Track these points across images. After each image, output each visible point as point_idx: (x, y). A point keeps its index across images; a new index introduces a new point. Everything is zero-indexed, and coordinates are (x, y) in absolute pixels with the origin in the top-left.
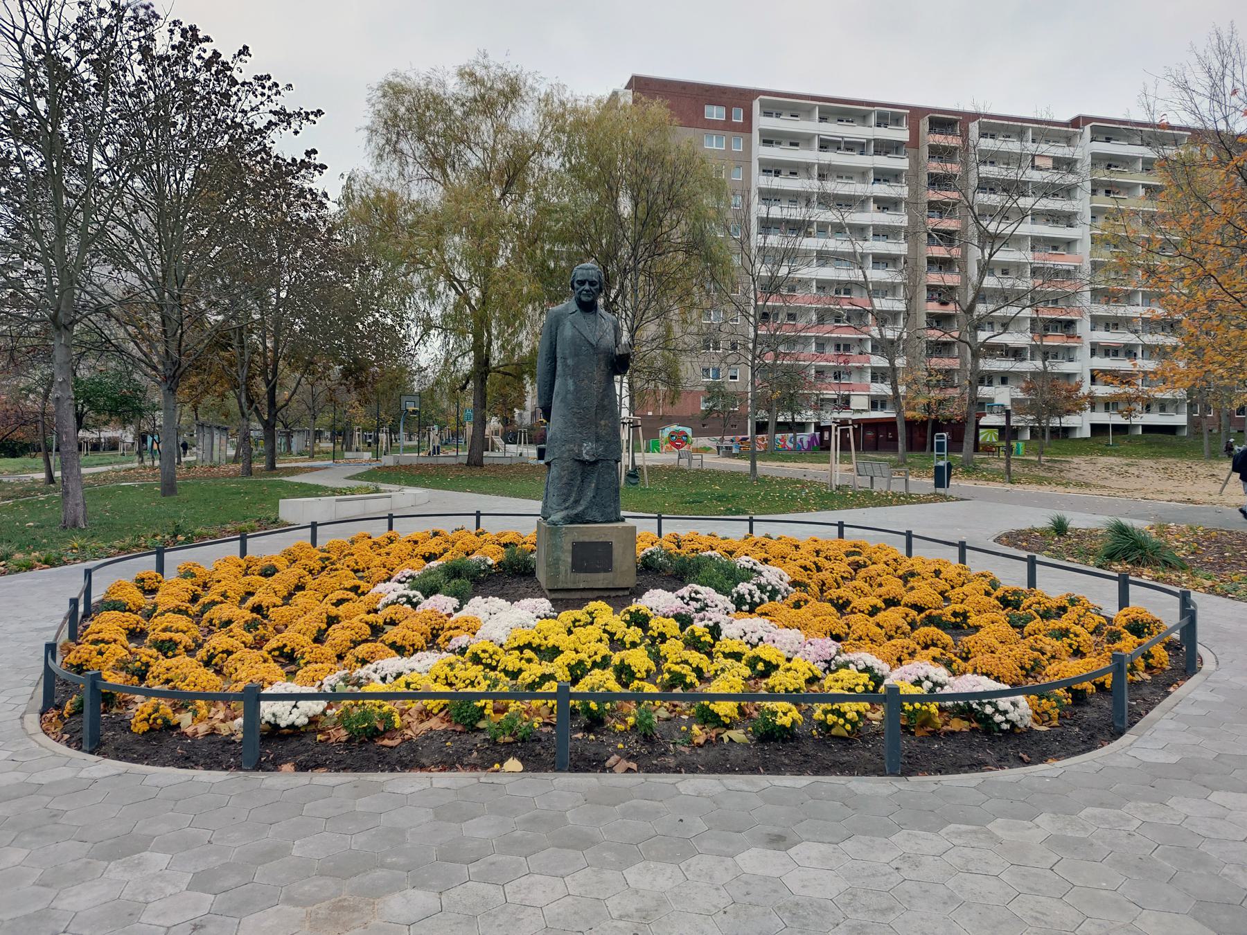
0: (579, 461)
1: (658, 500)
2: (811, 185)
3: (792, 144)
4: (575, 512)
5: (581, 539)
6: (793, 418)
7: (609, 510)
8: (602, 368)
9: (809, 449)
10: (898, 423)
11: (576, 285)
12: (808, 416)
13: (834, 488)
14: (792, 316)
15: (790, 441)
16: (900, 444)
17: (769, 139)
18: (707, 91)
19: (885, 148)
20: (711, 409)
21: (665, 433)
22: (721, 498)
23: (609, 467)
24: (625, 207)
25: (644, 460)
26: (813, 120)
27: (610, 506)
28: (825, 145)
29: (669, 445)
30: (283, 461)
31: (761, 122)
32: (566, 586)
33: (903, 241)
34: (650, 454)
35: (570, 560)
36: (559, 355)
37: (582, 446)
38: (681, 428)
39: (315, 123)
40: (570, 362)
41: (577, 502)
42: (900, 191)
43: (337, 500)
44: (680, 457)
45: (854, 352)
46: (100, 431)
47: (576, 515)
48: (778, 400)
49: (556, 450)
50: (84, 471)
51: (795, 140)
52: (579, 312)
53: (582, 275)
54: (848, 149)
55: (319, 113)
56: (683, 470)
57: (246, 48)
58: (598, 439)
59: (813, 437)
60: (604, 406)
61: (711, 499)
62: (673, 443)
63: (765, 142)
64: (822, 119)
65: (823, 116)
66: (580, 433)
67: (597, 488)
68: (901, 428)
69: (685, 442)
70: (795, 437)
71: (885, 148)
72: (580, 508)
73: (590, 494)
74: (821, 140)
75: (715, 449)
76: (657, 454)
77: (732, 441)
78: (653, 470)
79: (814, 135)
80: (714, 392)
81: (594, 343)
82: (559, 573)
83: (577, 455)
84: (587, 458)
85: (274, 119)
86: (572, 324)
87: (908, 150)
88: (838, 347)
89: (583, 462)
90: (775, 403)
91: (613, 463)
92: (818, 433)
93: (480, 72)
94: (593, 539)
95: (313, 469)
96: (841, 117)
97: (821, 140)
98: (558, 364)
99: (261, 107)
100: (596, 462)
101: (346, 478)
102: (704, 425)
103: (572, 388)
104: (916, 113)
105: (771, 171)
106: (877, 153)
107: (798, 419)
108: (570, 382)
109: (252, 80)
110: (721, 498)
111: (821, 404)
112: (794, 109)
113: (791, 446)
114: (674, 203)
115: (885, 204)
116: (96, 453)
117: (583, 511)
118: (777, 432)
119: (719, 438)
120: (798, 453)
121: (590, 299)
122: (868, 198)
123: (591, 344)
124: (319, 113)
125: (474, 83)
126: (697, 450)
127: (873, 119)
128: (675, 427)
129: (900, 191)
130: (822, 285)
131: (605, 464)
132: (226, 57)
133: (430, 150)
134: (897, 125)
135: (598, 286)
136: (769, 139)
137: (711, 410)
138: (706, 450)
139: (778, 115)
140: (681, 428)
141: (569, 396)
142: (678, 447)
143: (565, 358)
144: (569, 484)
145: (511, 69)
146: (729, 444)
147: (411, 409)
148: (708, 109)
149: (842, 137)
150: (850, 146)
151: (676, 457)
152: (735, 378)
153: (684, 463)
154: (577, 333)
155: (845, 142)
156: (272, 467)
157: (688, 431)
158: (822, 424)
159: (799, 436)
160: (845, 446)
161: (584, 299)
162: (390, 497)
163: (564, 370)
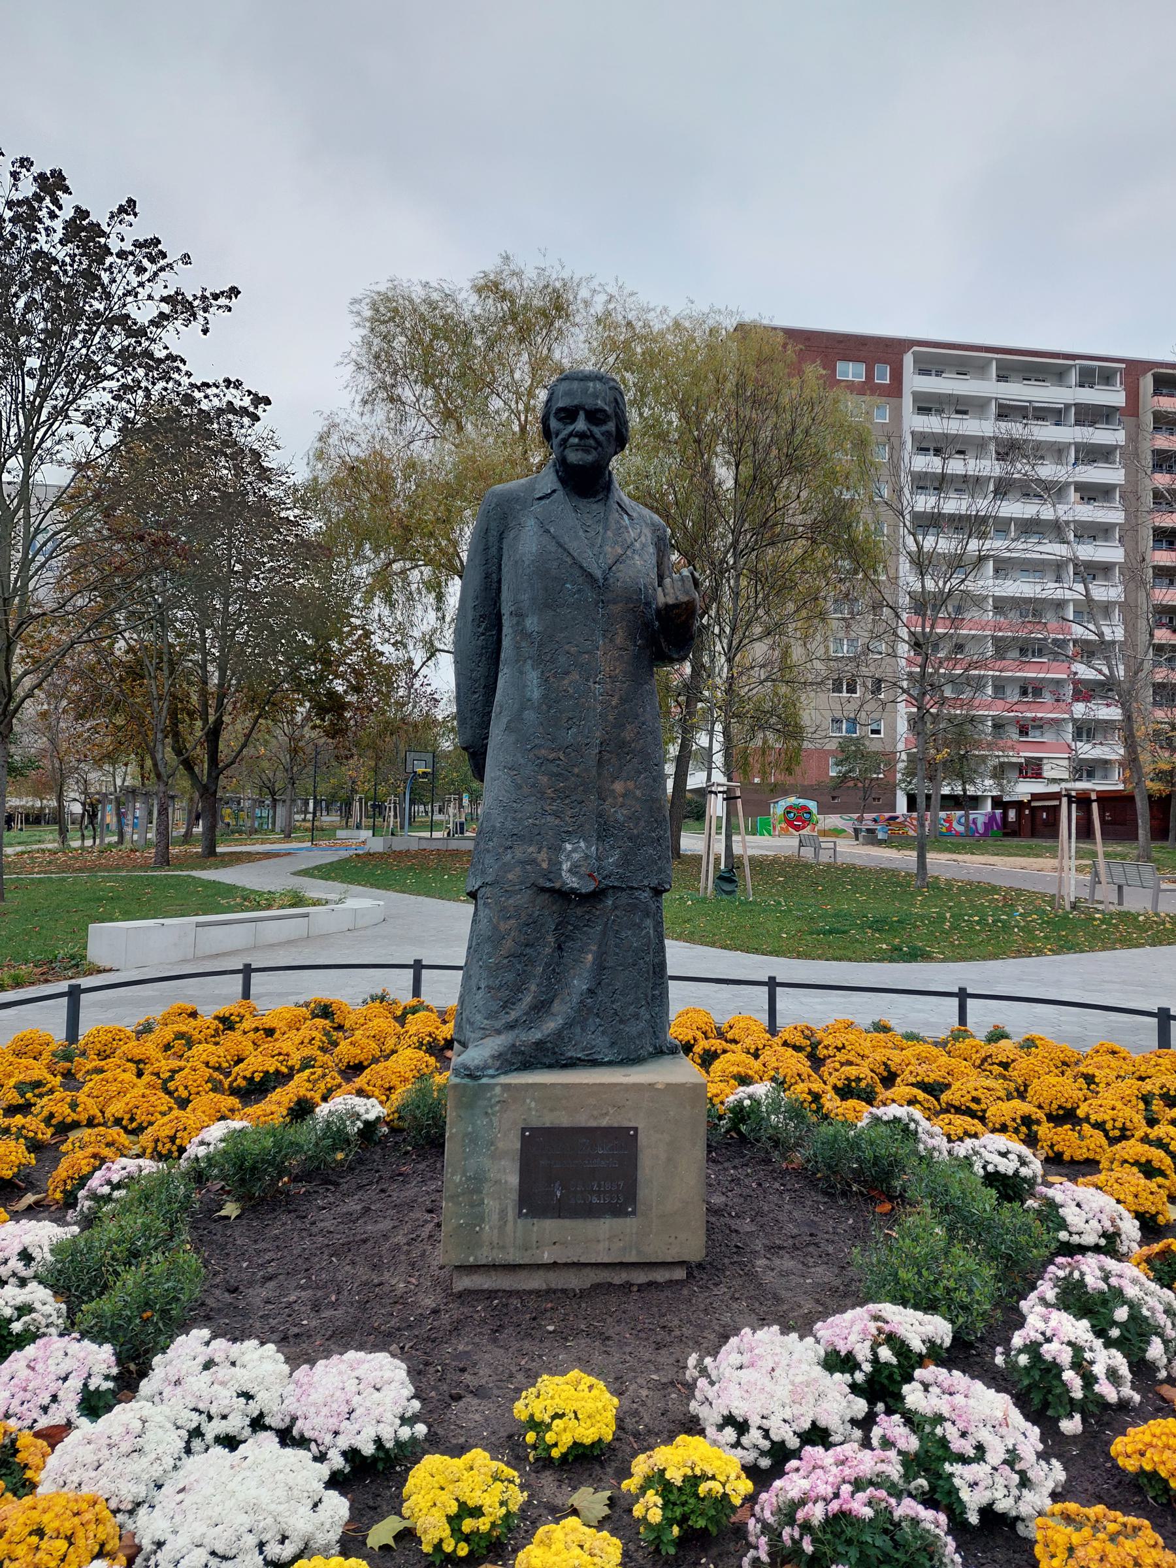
0: (552, 891)
1: (768, 925)
2: (988, 467)
3: (958, 412)
4: (536, 1035)
5: (549, 1119)
6: (964, 790)
7: (633, 1029)
8: (619, 640)
9: (985, 834)
10: (1138, 799)
11: (554, 424)
12: (986, 787)
13: (1068, 908)
14: (959, 648)
15: (959, 823)
16: (1140, 831)
17: (926, 405)
18: (840, 342)
19: (1090, 415)
20: (844, 776)
21: (779, 808)
22: (879, 925)
23: (633, 908)
24: (724, 475)
25: (745, 847)
26: (989, 379)
27: (636, 1016)
28: (1005, 412)
29: (784, 825)
30: (225, 842)
31: (915, 383)
32: (500, 1257)
33: (1117, 543)
34: (757, 838)
35: (514, 1180)
36: (506, 610)
37: (559, 849)
38: (802, 802)
39: (131, 225)
40: (532, 623)
41: (541, 1007)
42: (1110, 475)
43: (198, 925)
44: (801, 844)
45: (1047, 698)
46: (41, 800)
47: (539, 1044)
48: (944, 763)
49: (489, 860)
50: (9, 850)
51: (962, 406)
52: (560, 493)
53: (569, 393)
54: (1038, 419)
55: (234, 292)
56: (807, 866)
57: (132, 203)
58: (604, 831)
59: (992, 818)
60: (623, 744)
61: (862, 927)
62: (790, 823)
63: (920, 409)
64: (1001, 378)
65: (1002, 373)
66: (556, 815)
67: (600, 967)
68: (1142, 807)
69: (806, 822)
70: (967, 816)
71: (1090, 415)
72: (551, 1025)
73: (579, 983)
74: (1000, 406)
75: (851, 831)
76: (767, 837)
77: (875, 821)
78: (761, 865)
79: (990, 399)
80: (852, 752)
81: (598, 574)
82: (481, 1219)
83: (546, 875)
84: (572, 882)
85: (166, 308)
86: (542, 524)
87: (1124, 418)
88: (1024, 693)
89: (563, 895)
90: (940, 768)
91: (645, 895)
92: (998, 812)
93: (510, 284)
94: (583, 1120)
95: (249, 857)
96: (1027, 375)
97: (1000, 406)
98: (505, 631)
99: (140, 290)
100: (597, 895)
101: (294, 874)
102: (834, 798)
103: (536, 694)
104: (1134, 369)
105: (928, 450)
106: (1079, 422)
107: (971, 790)
108: (533, 676)
109: (132, 248)
110: (879, 925)
111: (1000, 772)
112: (961, 366)
113: (961, 829)
114: (793, 464)
115: (1092, 493)
116: (36, 828)
117: (559, 1034)
118: (943, 808)
119: (856, 816)
120: (971, 840)
121: (590, 458)
122: (1068, 484)
123: (590, 575)
124: (234, 292)
125: (503, 298)
126: (825, 833)
127: (1073, 377)
128: (792, 800)
129: (1110, 475)
130: (1002, 605)
131: (624, 899)
132: (99, 216)
133: (441, 398)
134: (1107, 384)
135: (611, 426)
136: (926, 405)
137: (844, 778)
138: (837, 832)
139: (939, 374)
140: (802, 802)
141: (530, 715)
142: (797, 828)
143: (519, 615)
144: (521, 957)
145: (556, 275)
146: (872, 826)
147: (420, 770)
148: (840, 365)
149: (1030, 402)
150: (1042, 414)
151: (796, 842)
152: (877, 732)
153: (808, 853)
154: (552, 547)
155: (1035, 409)
156: (210, 851)
157: (812, 805)
158: (1006, 799)
159: (973, 815)
160: (1085, 832)
161: (573, 457)
162: (306, 915)
163: (518, 648)
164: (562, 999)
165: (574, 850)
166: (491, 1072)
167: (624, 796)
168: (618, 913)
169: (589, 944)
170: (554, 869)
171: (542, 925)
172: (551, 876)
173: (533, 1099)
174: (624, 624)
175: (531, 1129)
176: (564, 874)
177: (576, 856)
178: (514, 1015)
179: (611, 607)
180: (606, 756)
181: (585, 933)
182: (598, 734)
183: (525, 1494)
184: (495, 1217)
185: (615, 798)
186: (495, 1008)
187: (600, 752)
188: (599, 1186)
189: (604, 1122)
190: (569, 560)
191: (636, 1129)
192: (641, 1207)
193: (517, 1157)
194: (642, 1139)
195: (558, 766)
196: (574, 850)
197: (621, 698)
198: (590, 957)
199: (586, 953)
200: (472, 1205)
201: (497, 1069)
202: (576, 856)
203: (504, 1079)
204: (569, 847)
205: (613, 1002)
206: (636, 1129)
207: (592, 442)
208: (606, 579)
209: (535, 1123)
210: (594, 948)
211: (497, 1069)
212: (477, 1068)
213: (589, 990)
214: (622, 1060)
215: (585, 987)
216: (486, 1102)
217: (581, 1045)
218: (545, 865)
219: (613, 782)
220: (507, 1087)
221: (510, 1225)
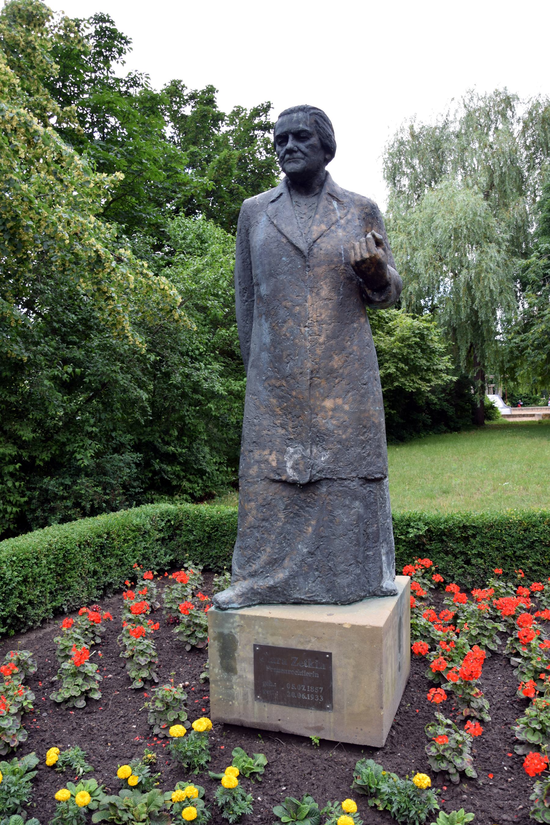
0: (280, 481)
4: (271, 582)
5: (280, 642)
37: (283, 452)
52: (285, 196)
60: (331, 371)
66: (283, 426)
72: (281, 575)
81: (303, 246)
83: (276, 471)
94: (294, 644)
117: (286, 582)
123: (297, 249)
131: (336, 487)
164: (291, 558)
165: (295, 453)
166: (235, 605)
167: (334, 410)
168: (331, 498)
169: (309, 520)
170: (281, 466)
171: (275, 506)
172: (279, 471)
173: (260, 626)
174: (328, 280)
175: (260, 646)
176: (288, 470)
177: (296, 456)
178: (255, 567)
179: (316, 269)
180: (317, 381)
181: (308, 512)
182: (309, 365)
183: (31, 707)
184: (241, 697)
185: (326, 412)
186: (243, 562)
187: (311, 379)
188: (306, 688)
189: (308, 647)
190: (284, 240)
191: (330, 654)
192: (336, 706)
193: (252, 662)
194: (335, 661)
195: (282, 390)
196: (295, 453)
197: (327, 337)
198: (310, 529)
199: (308, 526)
200: (226, 688)
201: (240, 604)
202: (296, 456)
203: (246, 612)
204: (291, 450)
205: (328, 561)
206: (330, 654)
207: (299, 154)
208: (310, 249)
209: (263, 643)
210: (313, 523)
211: (240, 604)
212: (224, 603)
213: (309, 552)
214: (336, 601)
215: (305, 550)
216: (230, 625)
217: (304, 590)
218: (274, 464)
219: (323, 400)
220: (242, 617)
221: (250, 704)
